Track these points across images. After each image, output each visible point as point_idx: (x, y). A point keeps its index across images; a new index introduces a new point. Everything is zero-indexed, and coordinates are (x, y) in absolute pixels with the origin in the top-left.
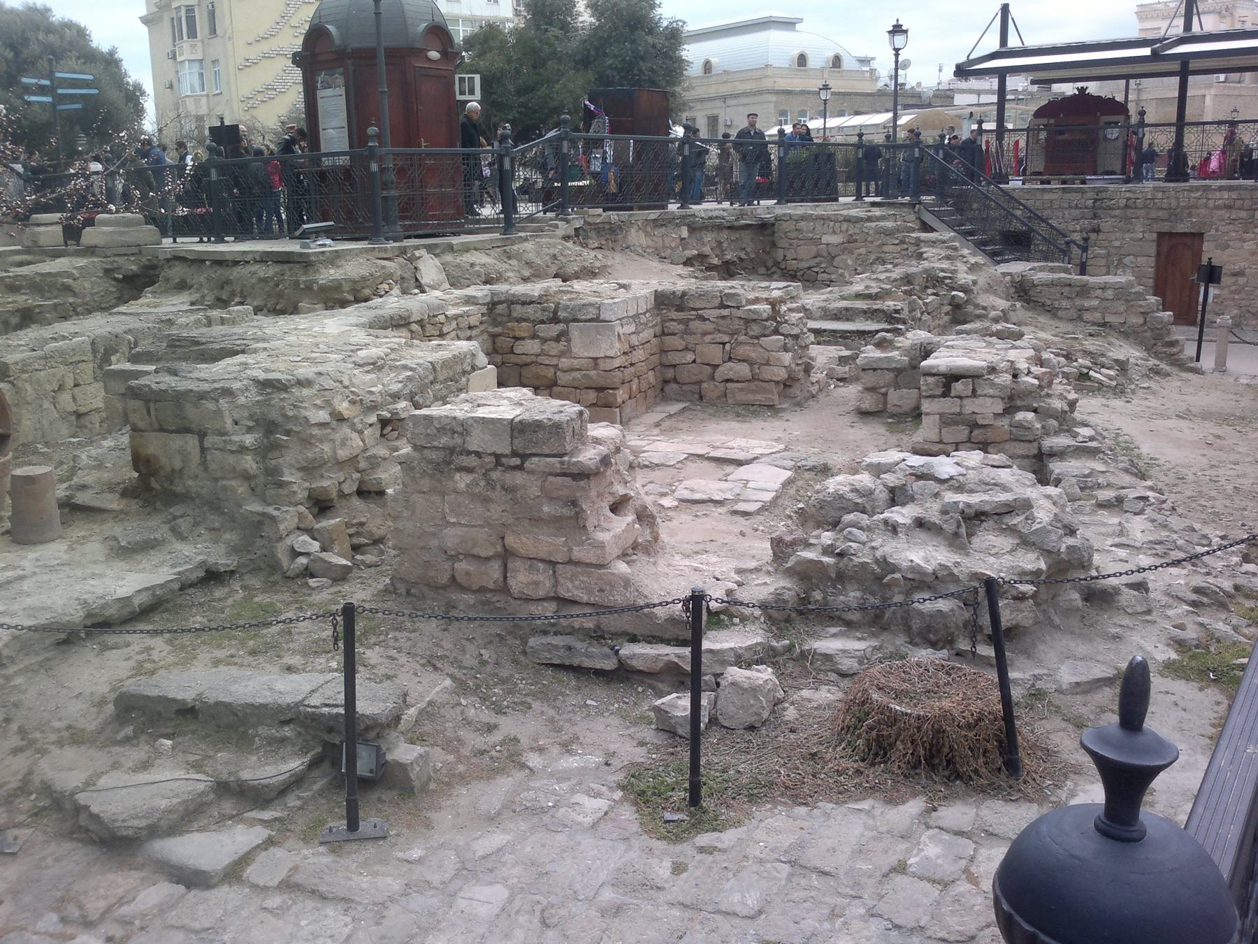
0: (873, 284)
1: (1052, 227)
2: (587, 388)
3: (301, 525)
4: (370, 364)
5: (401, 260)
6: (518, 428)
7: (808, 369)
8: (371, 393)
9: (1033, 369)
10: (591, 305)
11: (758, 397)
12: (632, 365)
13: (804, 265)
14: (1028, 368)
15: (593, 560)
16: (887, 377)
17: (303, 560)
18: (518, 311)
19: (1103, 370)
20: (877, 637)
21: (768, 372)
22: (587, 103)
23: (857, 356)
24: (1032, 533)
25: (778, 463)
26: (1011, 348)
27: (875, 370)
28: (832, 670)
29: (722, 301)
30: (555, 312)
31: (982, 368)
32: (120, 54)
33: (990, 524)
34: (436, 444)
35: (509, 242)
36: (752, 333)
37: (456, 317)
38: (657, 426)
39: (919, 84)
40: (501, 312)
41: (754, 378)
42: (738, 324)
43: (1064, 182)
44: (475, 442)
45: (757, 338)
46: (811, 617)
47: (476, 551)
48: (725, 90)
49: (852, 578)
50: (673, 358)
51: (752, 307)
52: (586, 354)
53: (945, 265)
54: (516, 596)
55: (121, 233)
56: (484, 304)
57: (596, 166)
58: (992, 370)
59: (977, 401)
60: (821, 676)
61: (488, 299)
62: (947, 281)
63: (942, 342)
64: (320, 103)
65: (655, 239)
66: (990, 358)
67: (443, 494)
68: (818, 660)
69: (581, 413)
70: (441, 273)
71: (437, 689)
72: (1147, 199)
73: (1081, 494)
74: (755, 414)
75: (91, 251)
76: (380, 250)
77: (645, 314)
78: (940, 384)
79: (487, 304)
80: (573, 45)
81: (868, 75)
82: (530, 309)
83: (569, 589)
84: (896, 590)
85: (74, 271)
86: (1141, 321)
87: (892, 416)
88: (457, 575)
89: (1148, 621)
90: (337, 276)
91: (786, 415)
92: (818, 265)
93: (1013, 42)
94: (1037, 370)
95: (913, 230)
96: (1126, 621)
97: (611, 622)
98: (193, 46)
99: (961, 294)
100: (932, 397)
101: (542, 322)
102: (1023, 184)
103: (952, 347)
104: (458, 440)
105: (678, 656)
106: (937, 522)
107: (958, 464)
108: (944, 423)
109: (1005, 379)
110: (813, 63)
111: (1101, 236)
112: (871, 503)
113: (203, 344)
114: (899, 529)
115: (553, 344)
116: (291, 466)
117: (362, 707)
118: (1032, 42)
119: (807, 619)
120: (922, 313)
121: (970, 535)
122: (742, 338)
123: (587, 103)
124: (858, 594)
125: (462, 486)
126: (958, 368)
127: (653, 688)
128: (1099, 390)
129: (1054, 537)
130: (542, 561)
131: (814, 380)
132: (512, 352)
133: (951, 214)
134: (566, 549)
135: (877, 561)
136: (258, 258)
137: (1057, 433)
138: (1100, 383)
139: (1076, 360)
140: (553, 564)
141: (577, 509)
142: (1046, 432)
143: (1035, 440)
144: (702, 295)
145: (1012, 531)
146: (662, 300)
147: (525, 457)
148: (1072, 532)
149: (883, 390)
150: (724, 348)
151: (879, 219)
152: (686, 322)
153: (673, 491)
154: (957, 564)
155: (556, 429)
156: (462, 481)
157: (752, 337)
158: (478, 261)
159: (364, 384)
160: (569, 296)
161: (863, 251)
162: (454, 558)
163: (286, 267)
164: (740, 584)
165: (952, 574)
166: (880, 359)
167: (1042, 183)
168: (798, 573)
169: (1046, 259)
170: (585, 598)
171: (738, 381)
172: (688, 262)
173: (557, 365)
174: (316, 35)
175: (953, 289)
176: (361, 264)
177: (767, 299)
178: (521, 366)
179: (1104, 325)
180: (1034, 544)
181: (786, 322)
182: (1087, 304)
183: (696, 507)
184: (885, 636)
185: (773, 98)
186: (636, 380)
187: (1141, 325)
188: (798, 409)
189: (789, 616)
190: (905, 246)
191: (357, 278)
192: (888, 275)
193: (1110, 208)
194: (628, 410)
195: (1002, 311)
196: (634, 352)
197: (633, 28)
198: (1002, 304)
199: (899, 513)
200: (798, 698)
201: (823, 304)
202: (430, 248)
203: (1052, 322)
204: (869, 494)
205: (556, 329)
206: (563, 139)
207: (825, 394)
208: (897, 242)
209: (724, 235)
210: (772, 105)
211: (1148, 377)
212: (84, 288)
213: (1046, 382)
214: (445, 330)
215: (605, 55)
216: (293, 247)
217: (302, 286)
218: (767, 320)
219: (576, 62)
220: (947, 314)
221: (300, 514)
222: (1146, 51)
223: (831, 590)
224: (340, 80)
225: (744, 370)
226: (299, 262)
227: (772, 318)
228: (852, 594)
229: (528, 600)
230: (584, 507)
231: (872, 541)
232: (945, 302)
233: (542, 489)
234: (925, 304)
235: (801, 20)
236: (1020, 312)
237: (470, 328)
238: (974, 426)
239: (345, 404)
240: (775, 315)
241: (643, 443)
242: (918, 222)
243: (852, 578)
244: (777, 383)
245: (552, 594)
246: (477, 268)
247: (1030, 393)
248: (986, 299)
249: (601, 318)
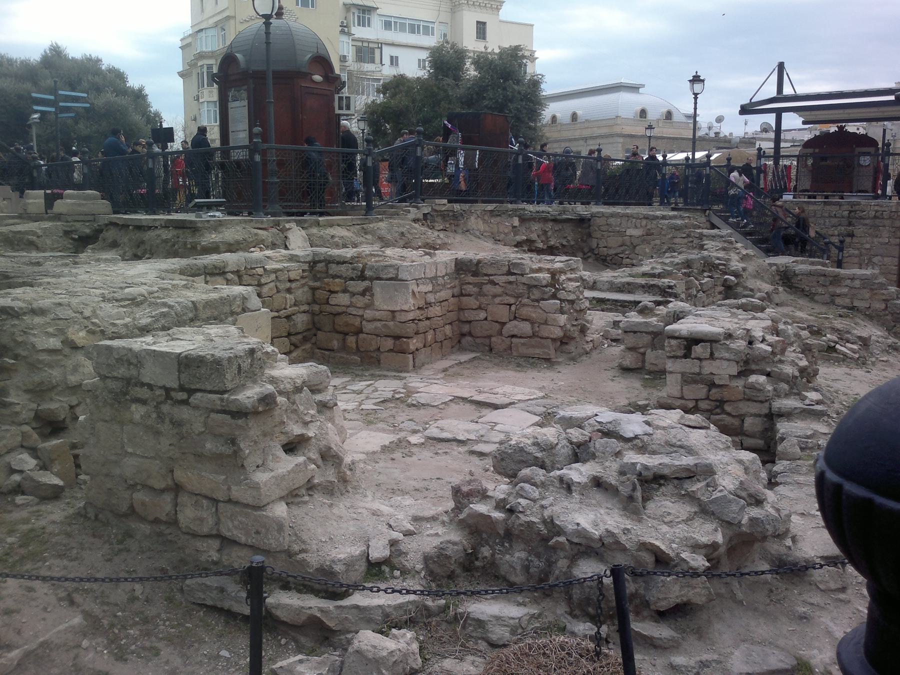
0: (659, 266)
2: (386, 336)
3: (25, 444)
4: (129, 300)
5: (274, 230)
7: (583, 330)
8: (114, 325)
9: (769, 338)
10: (391, 266)
11: (537, 351)
12: (428, 319)
13: (612, 252)
14: (763, 336)
15: (250, 501)
16: (645, 339)
17: (17, 478)
18: (334, 269)
19: (847, 344)
20: (538, 604)
21: (545, 331)
22: (446, 122)
24: (712, 502)
25: (531, 409)
26: (751, 319)
27: (635, 332)
28: (483, 639)
29: (509, 269)
30: (363, 271)
31: (719, 334)
32: (147, 91)
33: (669, 489)
34: (115, 374)
35: (367, 221)
36: (532, 297)
37: (275, 271)
38: (444, 371)
39: (731, 134)
40: (321, 270)
41: (534, 335)
42: (521, 289)
43: (826, 197)
44: (149, 374)
45: (538, 301)
46: (477, 574)
48: (586, 133)
49: (518, 537)
50: (469, 315)
51: (534, 275)
52: (385, 307)
53: (721, 254)
54: (184, 530)
55: (80, 205)
56: (305, 262)
57: (451, 169)
58: (729, 336)
60: (471, 644)
61: (309, 259)
62: (721, 267)
63: (693, 311)
64: (230, 112)
65: (491, 225)
66: (728, 325)
67: (122, 423)
68: (470, 625)
70: (306, 242)
71: (61, 627)
72: (891, 212)
73: (801, 454)
74: (533, 366)
75: (58, 217)
76: (257, 222)
77: (443, 276)
78: (682, 347)
79: (309, 262)
80: (460, 91)
82: (343, 268)
83: (229, 529)
84: (562, 554)
85: (38, 231)
86: (883, 306)
87: (650, 373)
88: (135, 505)
89: (841, 601)
90: (217, 240)
91: (559, 368)
92: (623, 252)
93: (787, 90)
96: (817, 599)
98: (211, 92)
99: (733, 278)
100: (675, 357)
101: (352, 279)
102: (794, 198)
103: (700, 315)
104: (134, 372)
105: (321, 610)
106: (613, 482)
107: (648, 423)
108: (685, 381)
109: (741, 344)
111: (855, 240)
112: (552, 458)
113: (11, 278)
114: (573, 488)
115: (360, 298)
116: (18, 387)
118: (801, 90)
119: (473, 576)
120: (698, 291)
121: (645, 499)
122: (525, 301)
123: (446, 122)
124: (523, 555)
125: (137, 417)
126: (697, 333)
127: (296, 641)
128: (844, 360)
129: (734, 508)
130: (206, 497)
131: (589, 339)
132: (328, 303)
134: (225, 487)
135: (544, 522)
136: (163, 225)
137: (787, 395)
138: (845, 355)
139: (825, 336)
140: (215, 501)
141: (235, 448)
142: (778, 394)
143: (766, 401)
144: (494, 263)
145: (691, 497)
147: (191, 392)
148: (758, 502)
149: (642, 350)
150: (510, 309)
151: (671, 218)
153: (425, 429)
154: (626, 531)
156: (137, 412)
157: (533, 301)
158: (338, 234)
159: (109, 316)
160: (377, 259)
161: (658, 242)
162: (132, 487)
163: (180, 232)
164: (408, 534)
165: (618, 543)
166: (640, 324)
167: (809, 197)
168: (469, 526)
169: (810, 256)
170: (243, 540)
171: (521, 337)
173: (363, 316)
174: (228, 60)
175: (726, 274)
176: (238, 231)
177: (548, 270)
178: (335, 315)
179: (852, 308)
180: (713, 514)
181: (564, 289)
182: (838, 291)
183: (440, 445)
184: (547, 603)
185: (621, 140)
186: (432, 332)
187: (883, 310)
188: (572, 363)
189: (453, 572)
190: (691, 239)
191: (232, 242)
192: (672, 260)
193: (861, 218)
194: (421, 357)
195: (767, 293)
196: (431, 308)
197: (506, 79)
198: (767, 287)
199: (577, 470)
200: (438, 669)
201: (612, 279)
202: (299, 223)
203: (810, 305)
204: (549, 448)
205: (362, 285)
206: (417, 145)
207: (598, 351)
208: (685, 235)
209: (550, 225)
210: (620, 145)
211: (887, 352)
212: (46, 245)
213: (779, 350)
215: (484, 98)
216: (190, 217)
217: (189, 246)
218: (546, 286)
219: (462, 103)
220: (720, 293)
221: (24, 434)
222: (892, 98)
223: (498, 547)
224: (244, 95)
225: (526, 328)
226: (190, 228)
228: (517, 554)
229: (195, 535)
230: (242, 445)
231: (543, 498)
232: (718, 284)
233: (205, 424)
234: (701, 284)
235: (643, 86)
236: (783, 294)
237: (290, 281)
238: (712, 385)
239: (82, 334)
241: (422, 385)
242: (708, 223)
243: (518, 537)
244: (554, 340)
245: (214, 532)
246: (336, 239)
247: (764, 358)
248: (752, 283)
249: (400, 277)
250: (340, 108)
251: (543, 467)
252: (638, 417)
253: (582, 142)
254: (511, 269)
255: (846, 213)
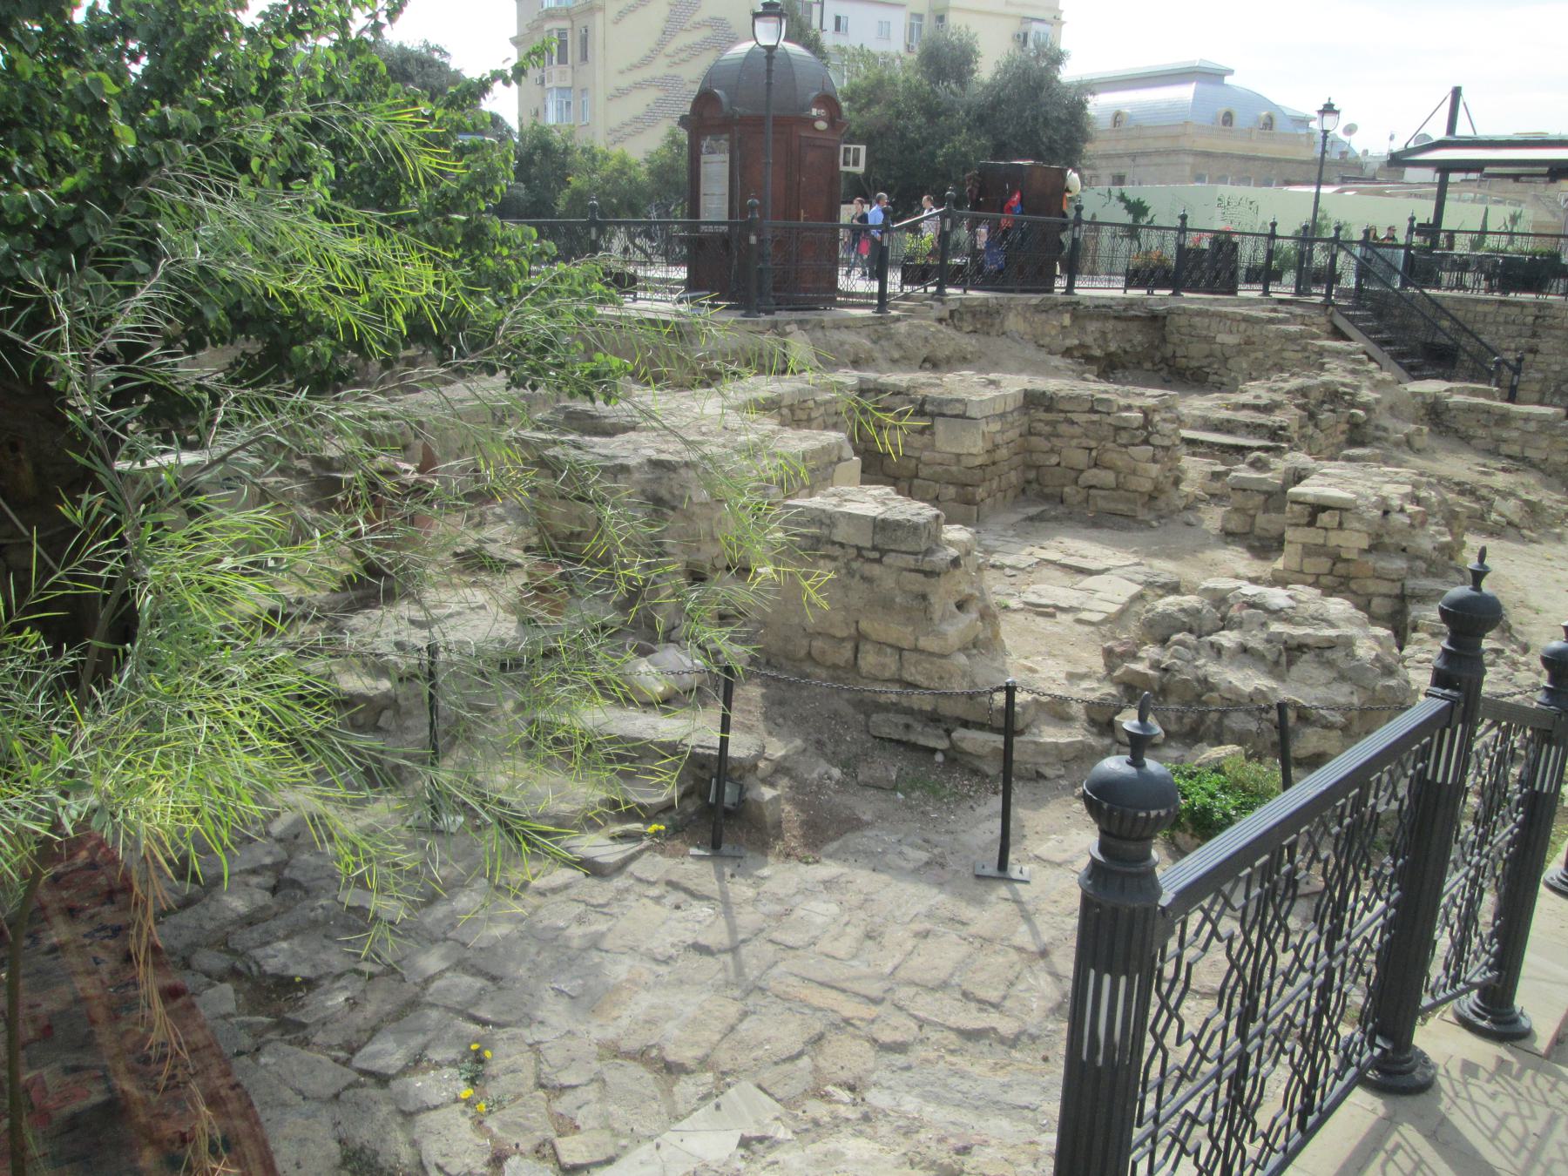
1: (1482, 343)
6: (881, 526)
12: (994, 463)
13: (1194, 364)
23: (1226, 473)
37: (826, 403)
41: (1118, 487)
45: (1125, 446)
47: (833, 631)
48: (1135, 146)
50: (1038, 458)
51: (1125, 414)
53: (1349, 379)
59: (1344, 534)
64: (704, 170)
69: (937, 516)
81: (1304, 139)
92: (1209, 365)
93: (1463, 130)
94: (1411, 508)
95: (1317, 337)
97: (948, 708)
99: (1361, 413)
100: (1297, 525)
104: (826, 531)
107: (1290, 597)
110: (1240, 121)
111: (1539, 358)
115: (917, 436)
117: (733, 752)
118: (1484, 132)
122: (1110, 445)
130: (891, 646)
133: (1366, 319)
135: (1198, 680)
140: (901, 650)
145: (1330, 664)
146: (1033, 401)
147: (884, 552)
151: (1280, 321)
152: (1053, 424)
154: (1274, 690)
155: (913, 529)
161: (1260, 355)
169: (1472, 379)
170: (925, 683)
171: (1102, 489)
172: (1068, 353)
174: (705, 99)
182: (1505, 435)
185: (1190, 160)
193: (1551, 327)
209: (1110, 325)
210: (1188, 168)
214: (813, 415)
220: (1343, 432)
227: (1144, 427)
229: (875, 679)
233: (898, 582)
235: (1230, 72)
238: (1337, 558)
240: (1147, 422)
244: (1142, 493)
250: (846, 163)
251: (1191, 631)
252: (1278, 591)
253: (1127, 161)
254: (1094, 406)
255: (1530, 319)
